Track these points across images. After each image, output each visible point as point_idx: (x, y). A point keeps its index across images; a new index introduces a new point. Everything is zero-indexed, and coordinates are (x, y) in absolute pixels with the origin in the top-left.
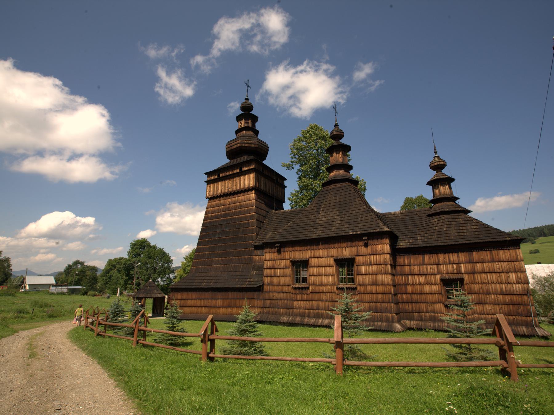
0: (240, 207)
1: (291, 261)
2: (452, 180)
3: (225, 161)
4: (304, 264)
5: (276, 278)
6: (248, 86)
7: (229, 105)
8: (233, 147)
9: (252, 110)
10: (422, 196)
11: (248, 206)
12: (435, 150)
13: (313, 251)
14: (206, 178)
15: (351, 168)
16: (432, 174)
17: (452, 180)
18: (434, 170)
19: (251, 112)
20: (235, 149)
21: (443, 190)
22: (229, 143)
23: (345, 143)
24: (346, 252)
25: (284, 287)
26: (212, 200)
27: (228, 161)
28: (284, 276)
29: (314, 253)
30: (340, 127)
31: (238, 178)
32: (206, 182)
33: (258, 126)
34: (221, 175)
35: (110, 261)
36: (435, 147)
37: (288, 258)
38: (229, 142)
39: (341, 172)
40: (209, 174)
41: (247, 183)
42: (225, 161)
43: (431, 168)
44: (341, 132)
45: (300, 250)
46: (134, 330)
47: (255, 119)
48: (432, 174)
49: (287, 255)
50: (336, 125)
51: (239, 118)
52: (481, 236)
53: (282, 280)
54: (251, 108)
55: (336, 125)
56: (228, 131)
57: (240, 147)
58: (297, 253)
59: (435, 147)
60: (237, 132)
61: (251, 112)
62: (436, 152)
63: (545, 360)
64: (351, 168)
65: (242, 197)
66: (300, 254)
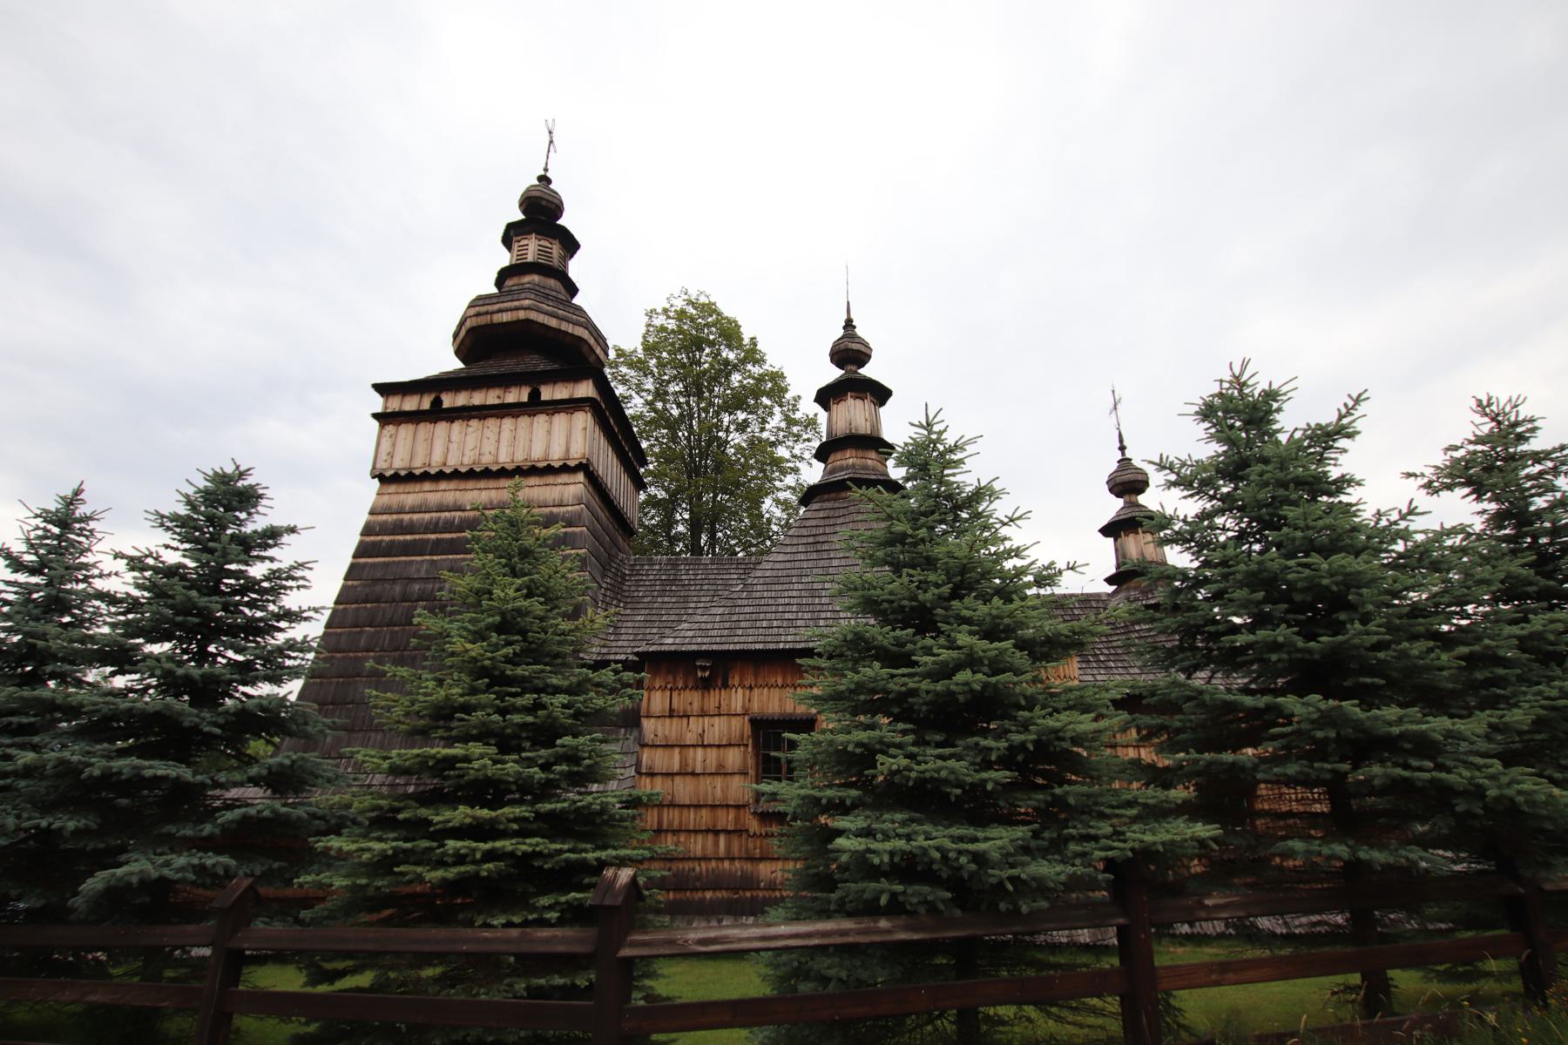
1: (753, 722)
5: (688, 779)
8: (498, 318)
12: (1121, 441)
14: (377, 403)
16: (1113, 506)
22: (480, 300)
24: (775, 700)
25: (721, 813)
26: (392, 488)
27: (460, 365)
28: (721, 772)
30: (859, 331)
31: (430, 426)
32: (376, 416)
33: (576, 269)
37: (739, 711)
38: (479, 298)
40: (384, 389)
43: (1111, 490)
46: (323, 899)
47: (570, 245)
48: (1113, 506)
49: (736, 699)
50: (849, 324)
53: (715, 789)
54: (556, 209)
55: (849, 324)
58: (776, 693)
62: (1122, 448)
65: (536, 491)
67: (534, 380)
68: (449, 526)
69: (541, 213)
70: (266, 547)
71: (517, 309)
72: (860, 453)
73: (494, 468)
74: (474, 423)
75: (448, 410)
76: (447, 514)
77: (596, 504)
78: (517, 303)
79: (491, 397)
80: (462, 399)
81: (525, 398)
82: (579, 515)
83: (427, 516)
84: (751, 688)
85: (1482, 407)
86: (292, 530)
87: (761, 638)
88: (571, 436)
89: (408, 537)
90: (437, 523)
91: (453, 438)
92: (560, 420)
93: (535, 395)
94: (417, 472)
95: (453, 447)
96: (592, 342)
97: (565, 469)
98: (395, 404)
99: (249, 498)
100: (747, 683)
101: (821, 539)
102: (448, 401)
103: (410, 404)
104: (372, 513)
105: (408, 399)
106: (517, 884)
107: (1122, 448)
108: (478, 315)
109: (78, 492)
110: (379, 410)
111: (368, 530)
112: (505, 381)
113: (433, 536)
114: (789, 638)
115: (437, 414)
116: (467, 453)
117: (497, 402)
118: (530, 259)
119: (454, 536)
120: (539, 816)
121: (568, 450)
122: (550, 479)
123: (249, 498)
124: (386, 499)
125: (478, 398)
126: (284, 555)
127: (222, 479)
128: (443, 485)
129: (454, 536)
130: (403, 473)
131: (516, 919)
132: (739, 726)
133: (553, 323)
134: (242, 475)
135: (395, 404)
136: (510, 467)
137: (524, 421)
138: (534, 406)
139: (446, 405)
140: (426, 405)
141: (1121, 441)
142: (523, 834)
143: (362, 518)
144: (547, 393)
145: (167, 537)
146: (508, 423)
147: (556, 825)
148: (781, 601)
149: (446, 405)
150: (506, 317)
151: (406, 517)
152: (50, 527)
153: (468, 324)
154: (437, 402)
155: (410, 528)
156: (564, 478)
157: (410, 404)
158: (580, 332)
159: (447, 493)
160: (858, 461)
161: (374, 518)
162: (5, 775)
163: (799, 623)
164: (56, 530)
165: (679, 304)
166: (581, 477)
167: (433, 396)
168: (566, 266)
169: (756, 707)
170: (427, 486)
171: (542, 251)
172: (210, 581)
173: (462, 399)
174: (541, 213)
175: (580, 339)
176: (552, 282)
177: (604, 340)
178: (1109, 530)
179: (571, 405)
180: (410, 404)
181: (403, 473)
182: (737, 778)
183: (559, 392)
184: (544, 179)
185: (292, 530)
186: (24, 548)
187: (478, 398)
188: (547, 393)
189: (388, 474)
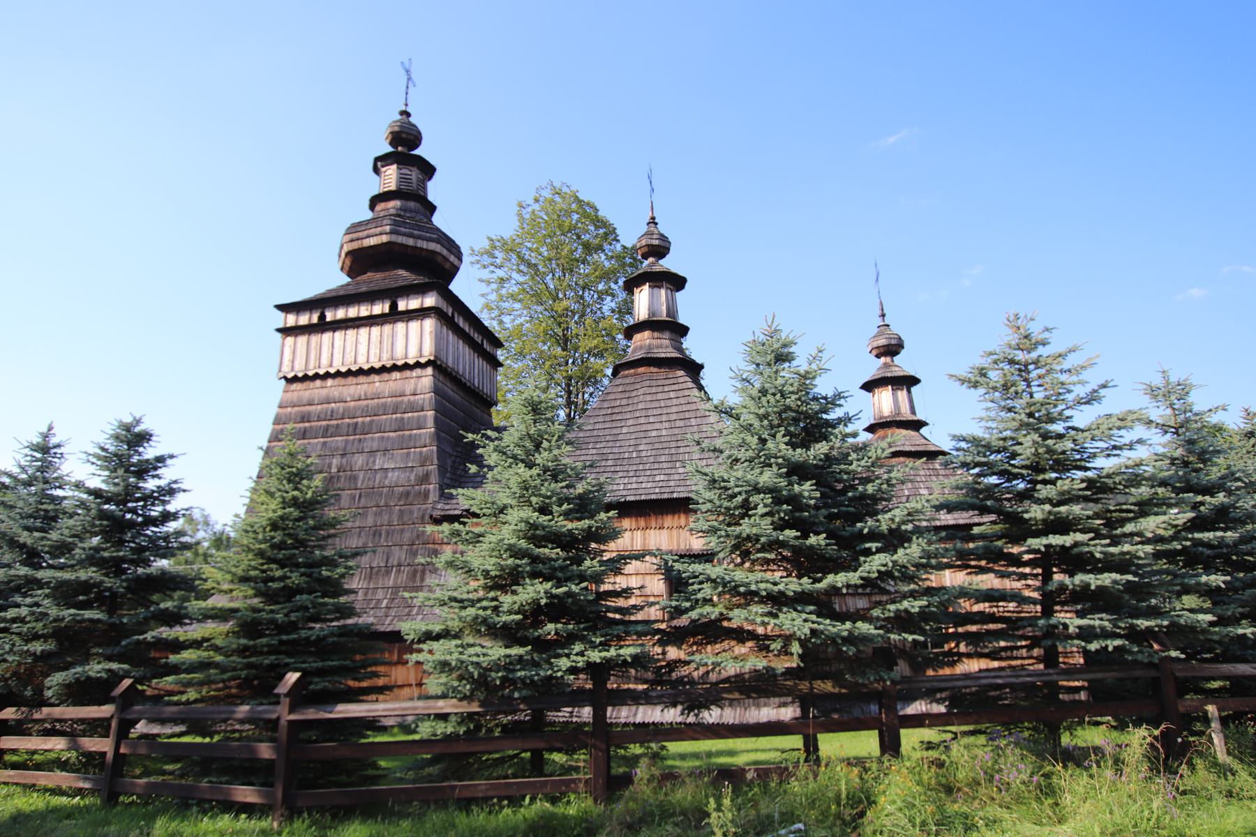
3: (337, 279)
6: (409, 79)
7: (112, 488)
9: (416, 147)
10: (701, 367)
11: (413, 408)
15: (683, 331)
19: (416, 152)
22: (355, 228)
23: (674, 270)
26: (295, 386)
27: (349, 280)
32: (279, 330)
33: (434, 191)
34: (586, 713)
40: (285, 308)
42: (337, 279)
44: (663, 238)
50: (653, 221)
51: (380, 162)
56: (347, 196)
57: (389, 243)
60: (375, 201)
61: (416, 152)
64: (683, 331)
65: (394, 382)
67: (392, 294)
69: (405, 144)
70: (156, 468)
72: (656, 334)
75: (331, 323)
77: (449, 390)
78: (379, 229)
79: (364, 311)
80: (340, 314)
81: (387, 310)
85: (1014, 322)
86: (172, 457)
88: (417, 339)
92: (414, 325)
93: (394, 306)
96: (445, 252)
97: (418, 365)
98: (291, 320)
99: (143, 438)
101: (616, 410)
103: (304, 319)
104: (280, 407)
108: (352, 241)
109: (50, 428)
110: (281, 325)
111: (277, 421)
112: (370, 297)
115: (323, 326)
118: (393, 187)
120: (282, 642)
122: (408, 373)
123: (143, 438)
124: (289, 395)
125: (352, 312)
126: (167, 474)
127: (128, 428)
128: (330, 382)
130: (300, 375)
133: (411, 242)
134: (138, 422)
135: (291, 320)
137: (387, 328)
138: (394, 316)
139: (328, 319)
140: (315, 319)
143: (273, 411)
144: (402, 305)
145: (93, 469)
146: (376, 330)
149: (328, 319)
152: (36, 454)
153: (346, 249)
156: (418, 372)
157: (313, 315)
158: (433, 246)
161: (281, 410)
162: (4, 620)
164: (39, 455)
165: (547, 194)
166: (429, 370)
168: (425, 188)
171: (402, 179)
172: (122, 499)
173: (340, 314)
174: (405, 144)
175: (434, 252)
176: (412, 204)
177: (458, 248)
179: (421, 313)
180: (304, 319)
183: (414, 303)
184: (406, 114)
185: (172, 457)
186: (18, 470)
187: (352, 312)
188: (402, 305)
189: (290, 376)
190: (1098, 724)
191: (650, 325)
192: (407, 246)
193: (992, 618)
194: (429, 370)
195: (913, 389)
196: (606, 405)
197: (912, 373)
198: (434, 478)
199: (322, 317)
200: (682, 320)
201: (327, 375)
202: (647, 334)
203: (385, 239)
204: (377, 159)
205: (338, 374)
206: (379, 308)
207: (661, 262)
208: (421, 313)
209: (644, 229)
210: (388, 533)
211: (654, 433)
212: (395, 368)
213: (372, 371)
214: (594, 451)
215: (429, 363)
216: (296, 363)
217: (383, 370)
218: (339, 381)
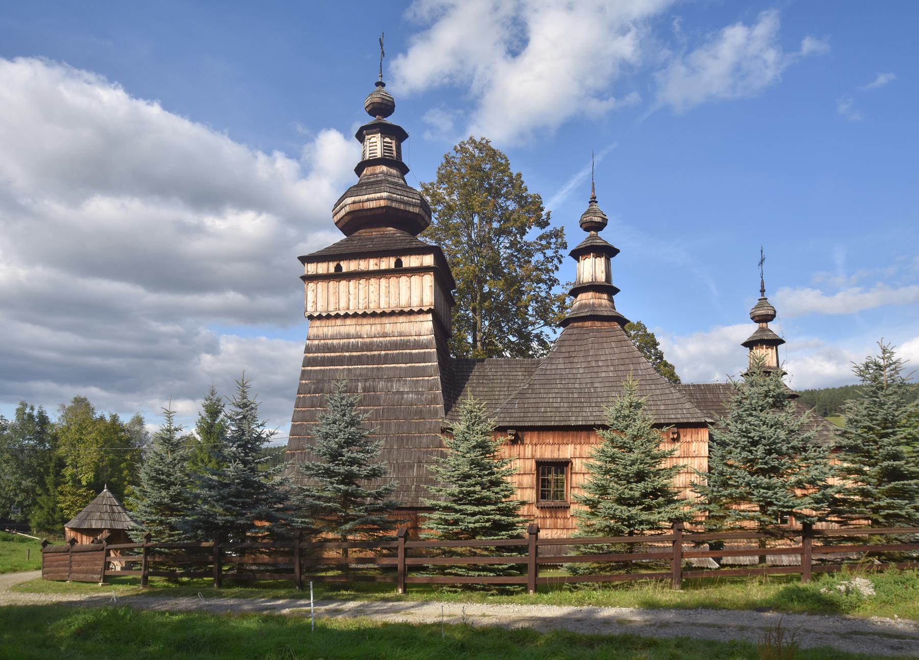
0: (405, 345)
2: (781, 342)
4: (562, 466)
11: (418, 345)
12: (763, 286)
13: (578, 447)
15: (615, 291)
17: (781, 342)
18: (756, 322)
20: (373, 209)
21: (768, 356)
24: (549, 450)
29: (581, 449)
35: (131, 97)
36: (762, 282)
37: (530, 456)
39: (603, 299)
41: (373, 297)
45: (554, 444)
48: (750, 330)
49: (528, 451)
50: (593, 201)
52: (531, 410)
58: (549, 448)
59: (762, 282)
62: (763, 291)
63: (367, 452)
66: (549, 450)
68: (356, 348)
71: (379, 199)
73: (379, 311)
74: (363, 281)
76: (353, 340)
78: (378, 195)
79: (371, 264)
81: (393, 266)
82: (430, 341)
83: (342, 341)
84: (536, 445)
87: (542, 419)
89: (332, 354)
90: (348, 346)
91: (351, 292)
92: (415, 279)
93: (399, 263)
94: (333, 314)
95: (351, 297)
100: (534, 442)
102: (348, 266)
103: (321, 268)
105: (320, 265)
106: (498, 527)
107: (763, 291)
113: (347, 354)
114: (557, 419)
115: (338, 275)
116: (361, 301)
117: (376, 268)
118: (379, 155)
119: (359, 353)
121: (422, 300)
122: (413, 318)
128: (348, 321)
129: (359, 353)
131: (857, 459)
132: (531, 465)
136: (388, 311)
137: (393, 280)
138: (399, 271)
139: (344, 270)
140: (332, 270)
141: (763, 286)
142: (495, 514)
146: (383, 281)
147: (501, 511)
148: (551, 395)
149: (344, 270)
150: (372, 205)
151: (330, 342)
154: (338, 268)
155: (332, 349)
156: (421, 317)
159: (350, 327)
160: (596, 301)
163: (562, 409)
167: (335, 263)
169: (538, 456)
170: (339, 322)
178: (750, 344)
179: (421, 270)
181: (324, 314)
182: (528, 490)
183: (410, 261)
190: (449, 616)
191: (593, 287)
192: (399, 210)
193: (57, 566)
194: (430, 317)
195: (780, 347)
196: (563, 349)
197: (781, 337)
198: (441, 398)
199: (338, 268)
200: (615, 284)
201: (346, 316)
202: (590, 294)
203: (382, 203)
204: (362, 129)
205: (355, 315)
206: (388, 263)
207: (600, 234)
208: (421, 270)
209: (586, 207)
210: (408, 440)
211: (603, 375)
212: (402, 313)
213: (383, 314)
214: (562, 386)
215: (428, 312)
216: (319, 304)
217: (393, 314)
218: (354, 321)
